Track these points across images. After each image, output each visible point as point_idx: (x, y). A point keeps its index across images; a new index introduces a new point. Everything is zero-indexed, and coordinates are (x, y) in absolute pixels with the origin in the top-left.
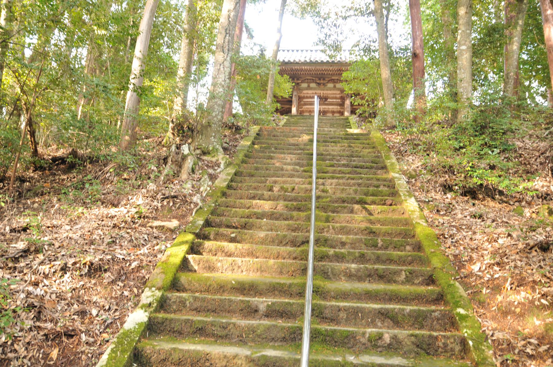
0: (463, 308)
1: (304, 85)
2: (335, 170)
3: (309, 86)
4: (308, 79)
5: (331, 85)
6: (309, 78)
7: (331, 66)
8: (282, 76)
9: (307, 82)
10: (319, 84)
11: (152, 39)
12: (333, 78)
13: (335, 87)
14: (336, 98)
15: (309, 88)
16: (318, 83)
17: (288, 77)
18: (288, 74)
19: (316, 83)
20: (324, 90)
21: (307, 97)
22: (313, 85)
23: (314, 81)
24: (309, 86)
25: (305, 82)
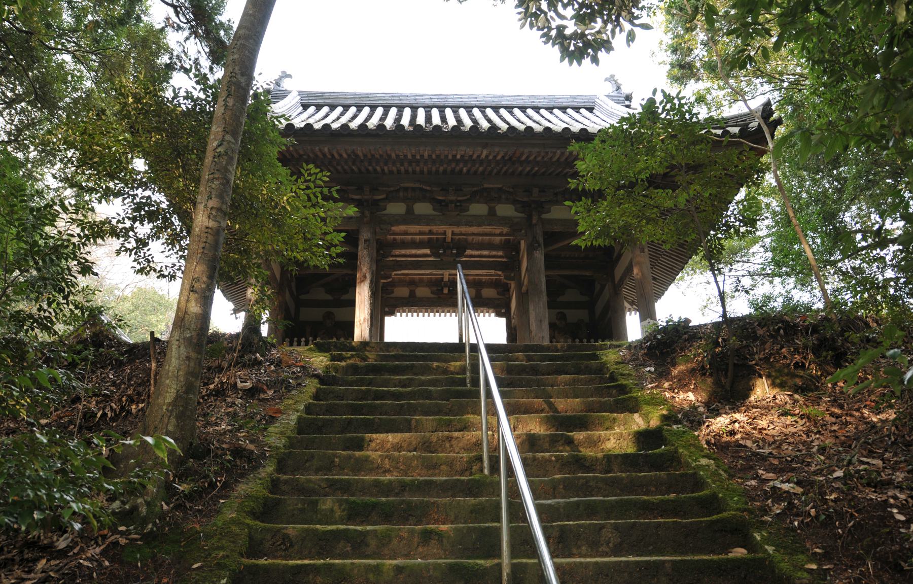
0: (231, 335)
1: (396, 208)
2: (362, 379)
3: (410, 211)
4: (406, 189)
5: (479, 209)
6: (411, 185)
7: (485, 146)
8: (297, 173)
9: (404, 200)
10: (441, 205)
11: (378, 261)
12: (486, 186)
13: (492, 212)
14: (490, 246)
15: (410, 217)
16: (440, 202)
17: (325, 176)
18: (321, 164)
19: (433, 200)
20: (458, 224)
21: (404, 245)
22: (423, 208)
23: (425, 196)
24: (410, 211)
25: (396, 200)
